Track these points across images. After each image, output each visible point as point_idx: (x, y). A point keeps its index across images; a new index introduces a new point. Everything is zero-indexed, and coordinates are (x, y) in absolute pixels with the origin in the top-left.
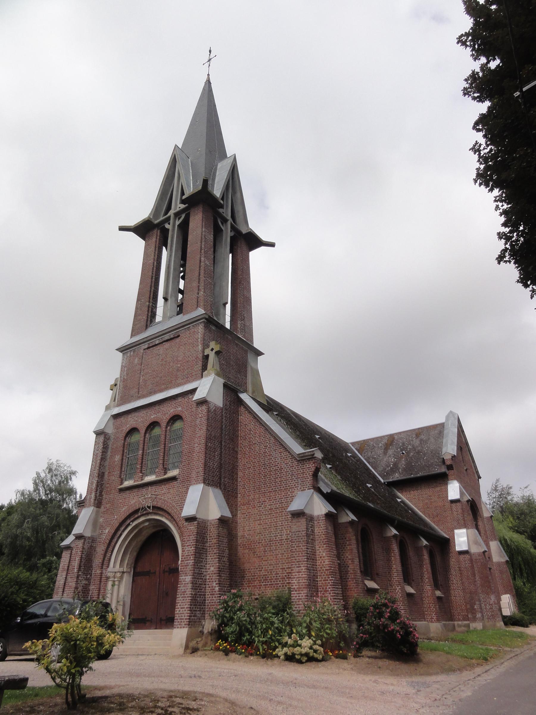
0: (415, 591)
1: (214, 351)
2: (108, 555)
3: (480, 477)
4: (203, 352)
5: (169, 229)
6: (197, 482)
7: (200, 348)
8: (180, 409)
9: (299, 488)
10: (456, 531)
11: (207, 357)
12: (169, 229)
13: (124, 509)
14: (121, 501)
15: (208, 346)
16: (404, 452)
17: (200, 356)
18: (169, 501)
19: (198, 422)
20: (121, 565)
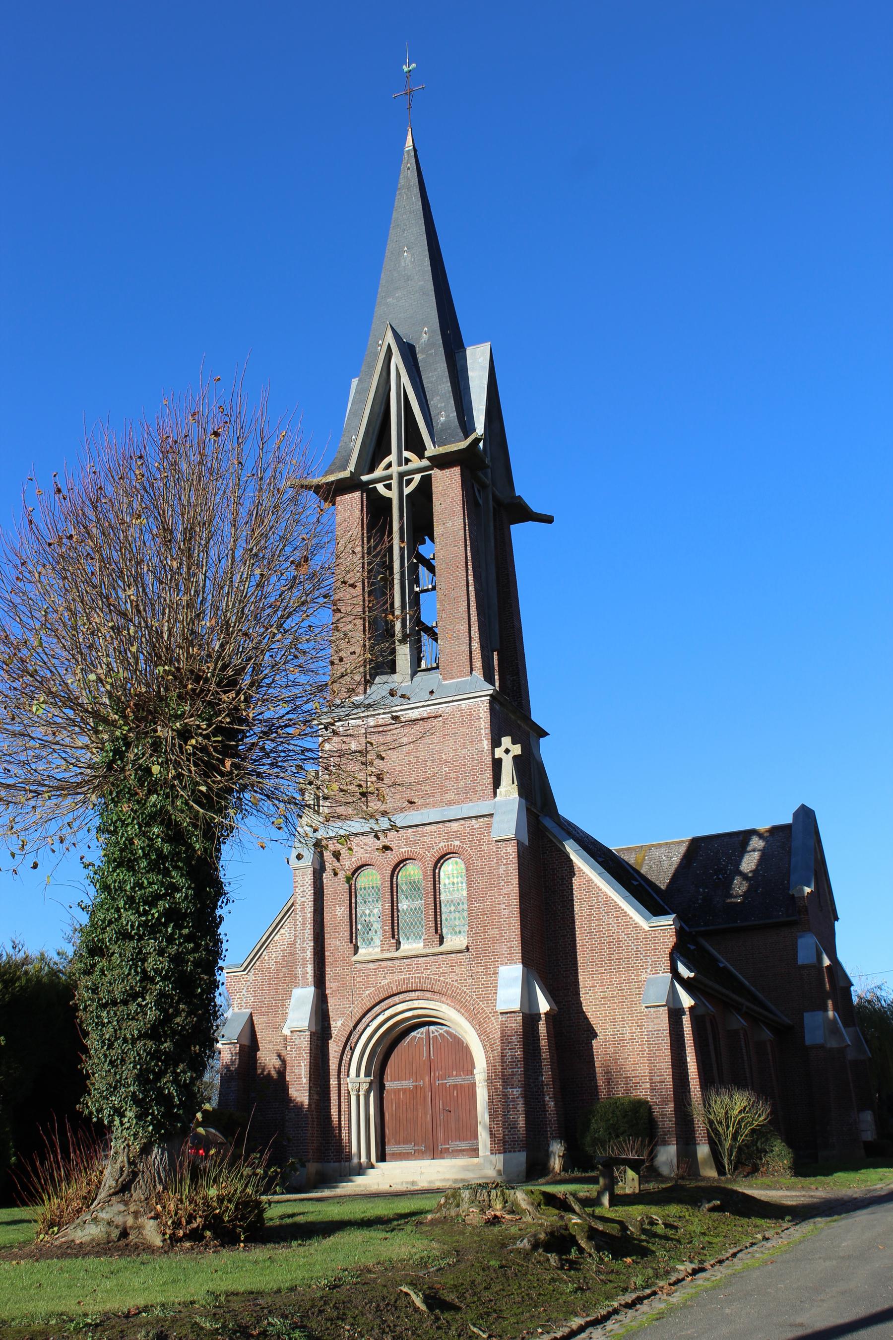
0: (309, 1105)
1: (511, 755)
2: (346, 1058)
3: (837, 919)
4: (493, 753)
5: (390, 500)
6: (511, 961)
7: (486, 744)
8: (457, 843)
9: (648, 971)
10: (807, 1016)
11: (500, 760)
12: (390, 500)
13: (367, 992)
14: (358, 979)
15: (499, 745)
16: (720, 876)
17: (488, 760)
18: (455, 984)
19: (501, 871)
20: (367, 1074)
